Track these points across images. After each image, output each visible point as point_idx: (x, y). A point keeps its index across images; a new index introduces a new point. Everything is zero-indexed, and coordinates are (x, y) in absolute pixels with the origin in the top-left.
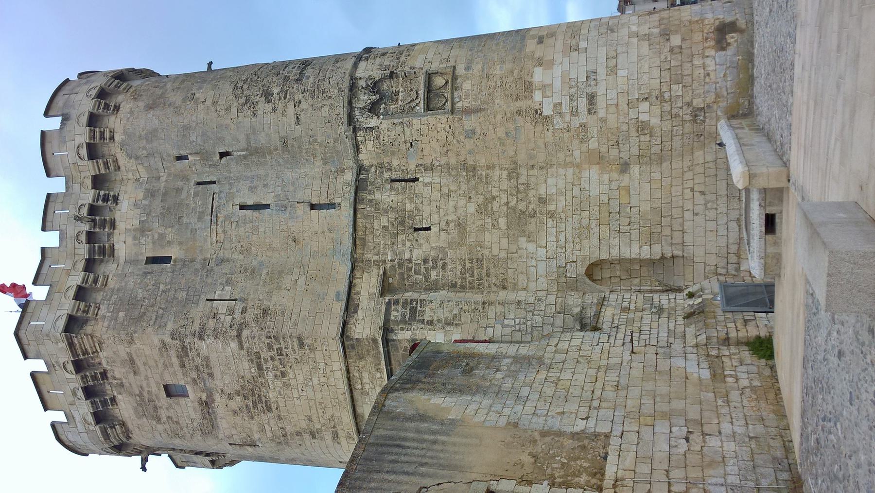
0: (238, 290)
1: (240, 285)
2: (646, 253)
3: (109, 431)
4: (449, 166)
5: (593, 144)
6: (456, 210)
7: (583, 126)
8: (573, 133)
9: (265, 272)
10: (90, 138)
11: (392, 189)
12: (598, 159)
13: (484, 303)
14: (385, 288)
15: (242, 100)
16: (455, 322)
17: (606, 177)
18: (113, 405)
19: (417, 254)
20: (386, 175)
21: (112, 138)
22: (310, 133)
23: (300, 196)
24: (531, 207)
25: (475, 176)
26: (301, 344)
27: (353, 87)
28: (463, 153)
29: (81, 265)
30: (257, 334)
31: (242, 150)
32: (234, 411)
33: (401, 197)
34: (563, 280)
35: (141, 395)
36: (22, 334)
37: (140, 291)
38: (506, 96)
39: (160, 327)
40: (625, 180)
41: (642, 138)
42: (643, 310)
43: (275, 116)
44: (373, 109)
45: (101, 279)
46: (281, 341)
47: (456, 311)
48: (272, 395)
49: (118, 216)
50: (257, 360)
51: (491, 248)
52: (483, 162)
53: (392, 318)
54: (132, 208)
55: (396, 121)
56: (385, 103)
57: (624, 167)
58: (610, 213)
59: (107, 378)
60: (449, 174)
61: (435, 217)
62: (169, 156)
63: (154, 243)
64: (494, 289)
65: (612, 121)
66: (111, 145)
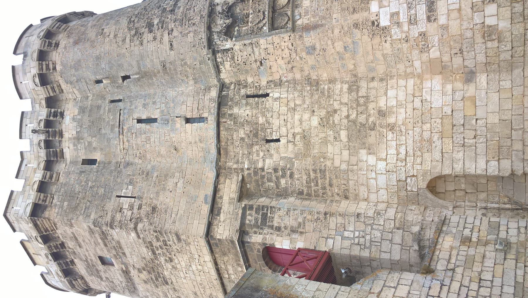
0: (137, 189)
1: (138, 185)
2: (493, 169)
3: (74, 282)
4: (295, 82)
5: (434, 53)
6: (301, 124)
7: (423, 35)
8: (412, 42)
9: (155, 175)
10: (39, 70)
11: (247, 104)
12: (440, 68)
13: (326, 214)
14: (243, 193)
15: (133, 32)
16: (300, 230)
17: (449, 87)
18: (72, 265)
19: (269, 163)
20: (243, 92)
21: (55, 69)
22: (182, 57)
24: (371, 119)
25: (317, 90)
26: (179, 239)
27: (211, 13)
28: (306, 68)
29: (42, 165)
30: (147, 228)
31: (136, 74)
32: (144, 281)
33: (254, 112)
34: (403, 193)
35: (86, 261)
36: (8, 215)
37: (77, 186)
38: (343, 10)
39: (87, 216)
40: (471, 90)
41: (489, 44)
42: (486, 243)
43: (155, 44)
44: (228, 32)
45: (55, 176)
46: (164, 235)
47: (300, 220)
48: (166, 273)
49: (64, 127)
50: (150, 245)
51: (333, 159)
52: (325, 76)
53: (247, 222)
54: (71, 121)
55: (247, 42)
56: (238, 26)
57: (470, 76)
58: (454, 126)
59: (65, 248)
60: (295, 89)
61: (284, 130)
62: (90, 80)
63: (85, 149)
64: (337, 198)
65: (455, 27)
66: (55, 74)
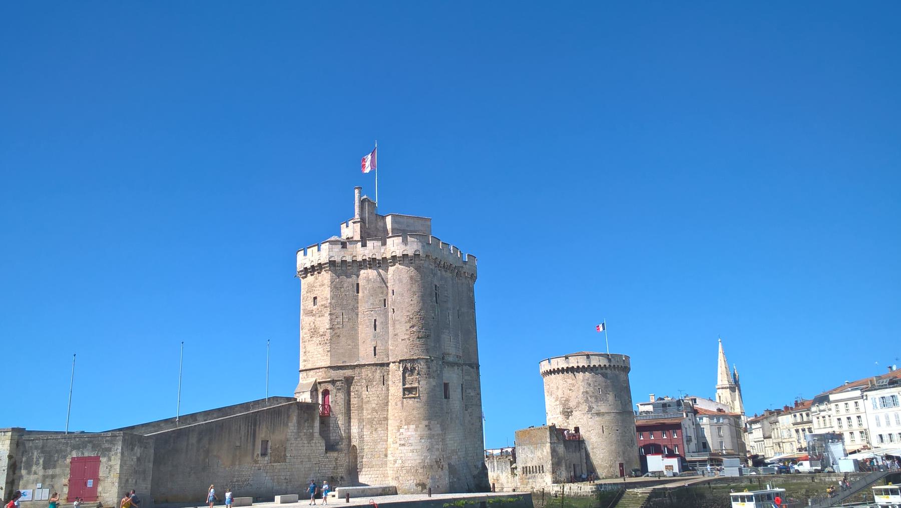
23: (379, 342)
